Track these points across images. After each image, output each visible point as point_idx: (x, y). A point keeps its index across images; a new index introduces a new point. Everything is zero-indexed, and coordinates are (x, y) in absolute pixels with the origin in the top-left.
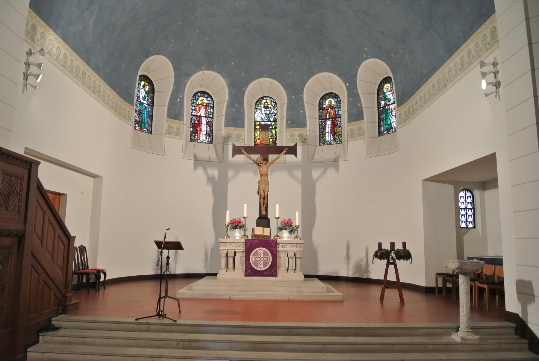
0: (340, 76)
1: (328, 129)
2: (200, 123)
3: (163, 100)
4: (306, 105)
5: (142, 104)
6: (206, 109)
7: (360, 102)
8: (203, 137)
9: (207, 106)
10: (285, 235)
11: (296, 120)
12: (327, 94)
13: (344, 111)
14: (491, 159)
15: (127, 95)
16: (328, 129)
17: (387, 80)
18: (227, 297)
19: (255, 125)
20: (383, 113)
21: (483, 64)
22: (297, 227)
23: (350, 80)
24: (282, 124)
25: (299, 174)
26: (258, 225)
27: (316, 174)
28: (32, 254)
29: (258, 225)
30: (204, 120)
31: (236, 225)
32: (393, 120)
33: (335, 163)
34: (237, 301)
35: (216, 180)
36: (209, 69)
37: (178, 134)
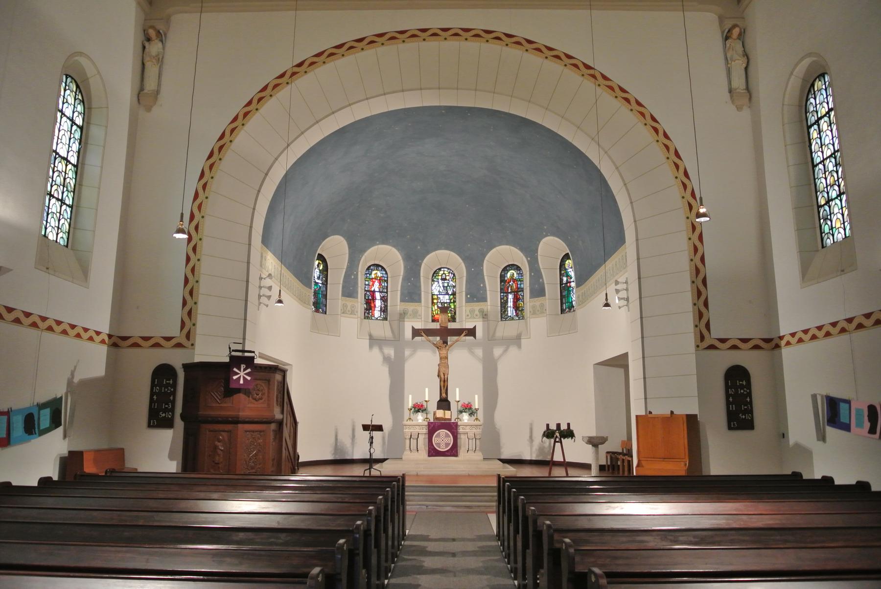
0: (521, 249)
1: (510, 304)
2: (374, 299)
3: (336, 278)
4: (486, 278)
5: (316, 283)
6: (380, 284)
7: (542, 277)
8: (377, 314)
9: (380, 280)
10: (465, 417)
11: (476, 294)
12: (509, 266)
13: (526, 285)
14: (626, 355)
15: (305, 278)
16: (510, 304)
17: (567, 257)
18: (415, 473)
19: (433, 299)
20: (565, 290)
21: (617, 283)
22: (477, 410)
23: (531, 253)
24: (461, 298)
25: (479, 352)
26: (438, 408)
27: (497, 351)
28: (531, 425)
29: (438, 408)
30: (378, 295)
31: (419, 408)
32: (574, 297)
33: (517, 340)
34: (423, 476)
35: (393, 357)
36: (383, 243)
37: (353, 312)
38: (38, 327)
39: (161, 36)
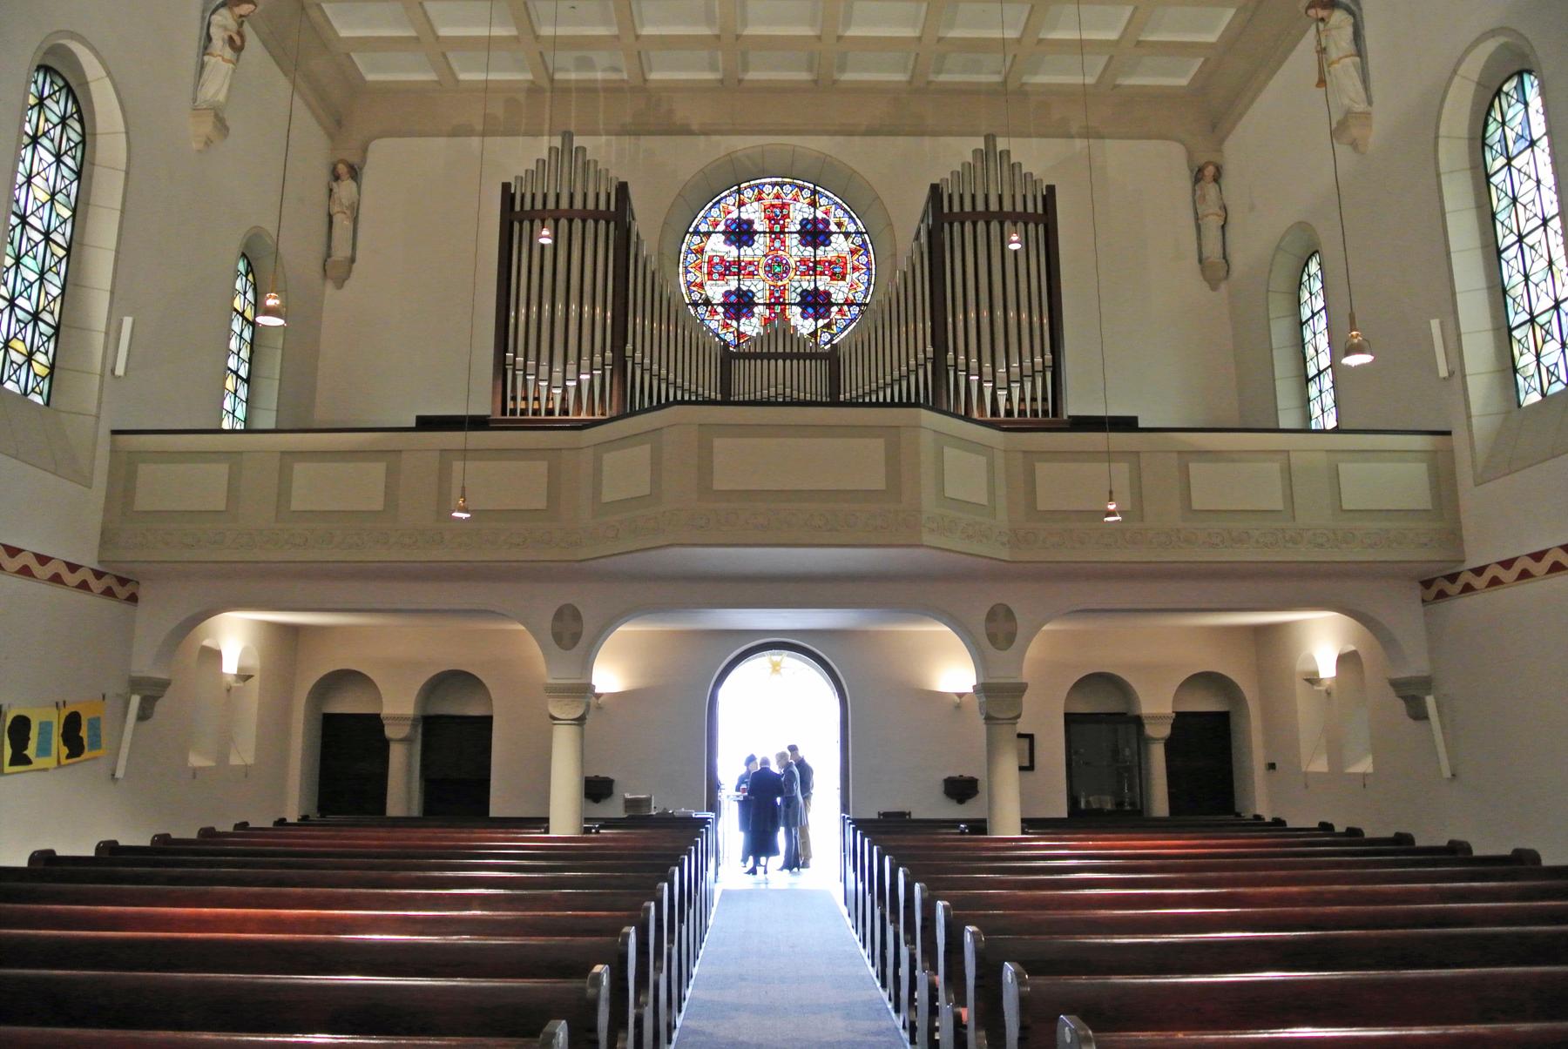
38: (62, 583)
39: (355, 173)
